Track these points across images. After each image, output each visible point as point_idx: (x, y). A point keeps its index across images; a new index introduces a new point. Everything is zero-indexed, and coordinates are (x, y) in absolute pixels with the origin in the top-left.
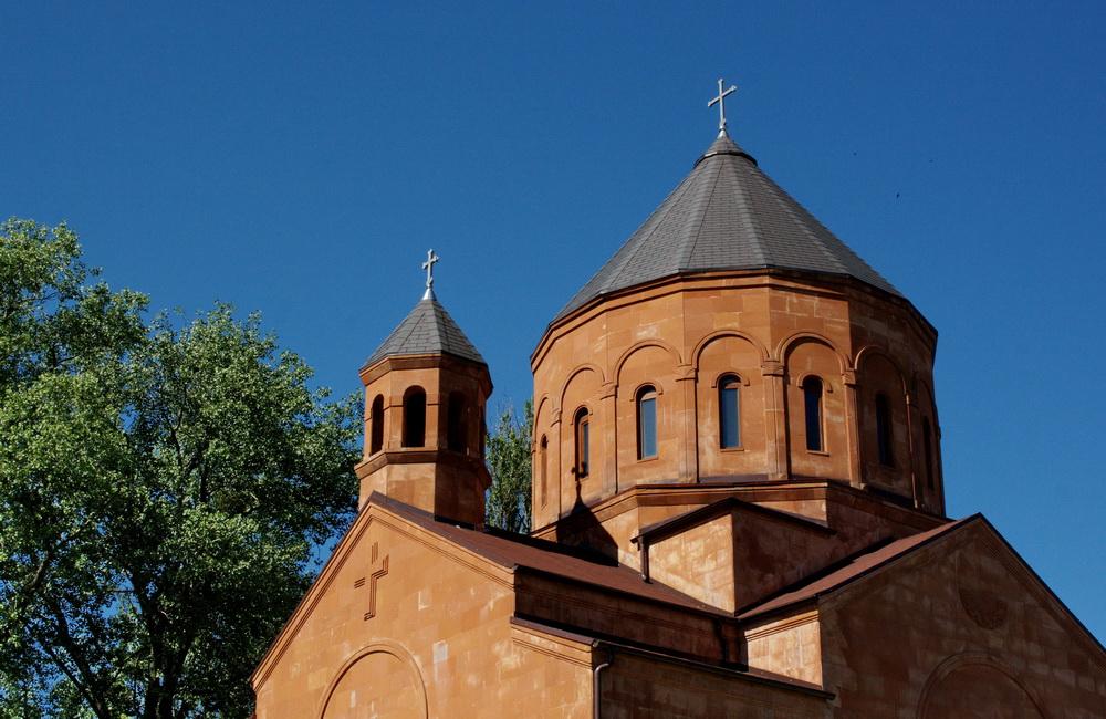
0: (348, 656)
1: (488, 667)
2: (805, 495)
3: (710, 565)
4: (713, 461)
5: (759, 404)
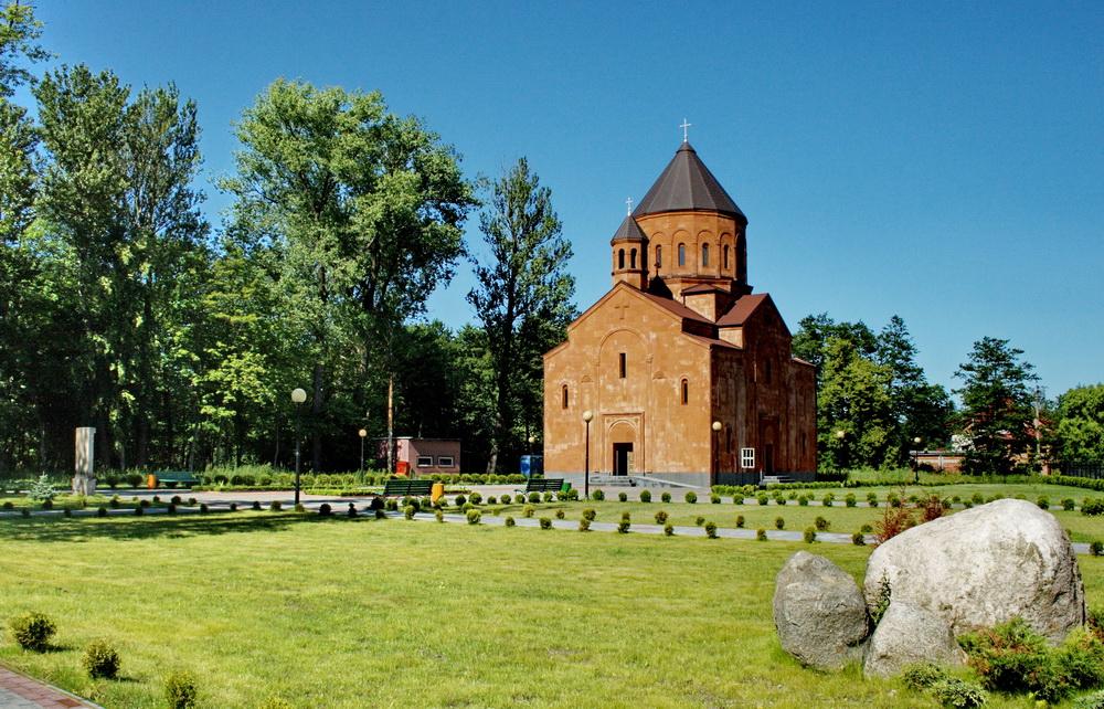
0: (613, 329)
1: (673, 344)
2: (726, 283)
3: (706, 307)
4: (701, 271)
5: (714, 253)
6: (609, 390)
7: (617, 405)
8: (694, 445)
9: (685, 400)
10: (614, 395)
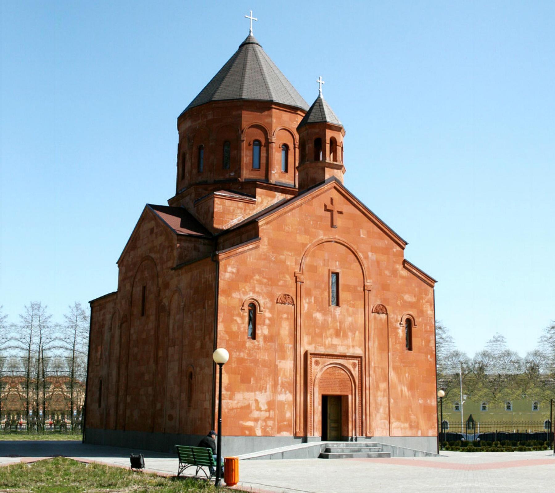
6: (315, 320)
7: (328, 341)
8: (421, 401)
9: (410, 347)
10: (324, 327)
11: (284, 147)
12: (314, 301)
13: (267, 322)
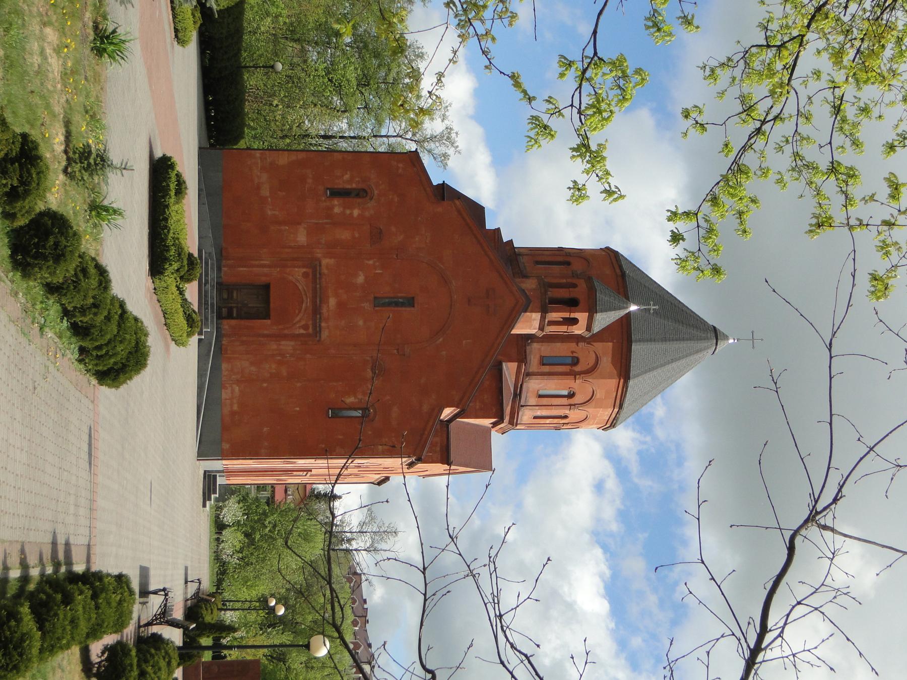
11: (572, 393)
12: (377, 273)
13: (348, 212)
